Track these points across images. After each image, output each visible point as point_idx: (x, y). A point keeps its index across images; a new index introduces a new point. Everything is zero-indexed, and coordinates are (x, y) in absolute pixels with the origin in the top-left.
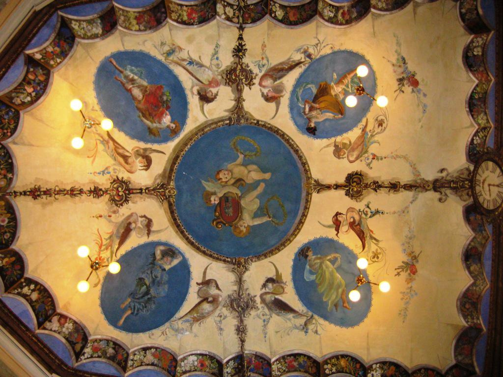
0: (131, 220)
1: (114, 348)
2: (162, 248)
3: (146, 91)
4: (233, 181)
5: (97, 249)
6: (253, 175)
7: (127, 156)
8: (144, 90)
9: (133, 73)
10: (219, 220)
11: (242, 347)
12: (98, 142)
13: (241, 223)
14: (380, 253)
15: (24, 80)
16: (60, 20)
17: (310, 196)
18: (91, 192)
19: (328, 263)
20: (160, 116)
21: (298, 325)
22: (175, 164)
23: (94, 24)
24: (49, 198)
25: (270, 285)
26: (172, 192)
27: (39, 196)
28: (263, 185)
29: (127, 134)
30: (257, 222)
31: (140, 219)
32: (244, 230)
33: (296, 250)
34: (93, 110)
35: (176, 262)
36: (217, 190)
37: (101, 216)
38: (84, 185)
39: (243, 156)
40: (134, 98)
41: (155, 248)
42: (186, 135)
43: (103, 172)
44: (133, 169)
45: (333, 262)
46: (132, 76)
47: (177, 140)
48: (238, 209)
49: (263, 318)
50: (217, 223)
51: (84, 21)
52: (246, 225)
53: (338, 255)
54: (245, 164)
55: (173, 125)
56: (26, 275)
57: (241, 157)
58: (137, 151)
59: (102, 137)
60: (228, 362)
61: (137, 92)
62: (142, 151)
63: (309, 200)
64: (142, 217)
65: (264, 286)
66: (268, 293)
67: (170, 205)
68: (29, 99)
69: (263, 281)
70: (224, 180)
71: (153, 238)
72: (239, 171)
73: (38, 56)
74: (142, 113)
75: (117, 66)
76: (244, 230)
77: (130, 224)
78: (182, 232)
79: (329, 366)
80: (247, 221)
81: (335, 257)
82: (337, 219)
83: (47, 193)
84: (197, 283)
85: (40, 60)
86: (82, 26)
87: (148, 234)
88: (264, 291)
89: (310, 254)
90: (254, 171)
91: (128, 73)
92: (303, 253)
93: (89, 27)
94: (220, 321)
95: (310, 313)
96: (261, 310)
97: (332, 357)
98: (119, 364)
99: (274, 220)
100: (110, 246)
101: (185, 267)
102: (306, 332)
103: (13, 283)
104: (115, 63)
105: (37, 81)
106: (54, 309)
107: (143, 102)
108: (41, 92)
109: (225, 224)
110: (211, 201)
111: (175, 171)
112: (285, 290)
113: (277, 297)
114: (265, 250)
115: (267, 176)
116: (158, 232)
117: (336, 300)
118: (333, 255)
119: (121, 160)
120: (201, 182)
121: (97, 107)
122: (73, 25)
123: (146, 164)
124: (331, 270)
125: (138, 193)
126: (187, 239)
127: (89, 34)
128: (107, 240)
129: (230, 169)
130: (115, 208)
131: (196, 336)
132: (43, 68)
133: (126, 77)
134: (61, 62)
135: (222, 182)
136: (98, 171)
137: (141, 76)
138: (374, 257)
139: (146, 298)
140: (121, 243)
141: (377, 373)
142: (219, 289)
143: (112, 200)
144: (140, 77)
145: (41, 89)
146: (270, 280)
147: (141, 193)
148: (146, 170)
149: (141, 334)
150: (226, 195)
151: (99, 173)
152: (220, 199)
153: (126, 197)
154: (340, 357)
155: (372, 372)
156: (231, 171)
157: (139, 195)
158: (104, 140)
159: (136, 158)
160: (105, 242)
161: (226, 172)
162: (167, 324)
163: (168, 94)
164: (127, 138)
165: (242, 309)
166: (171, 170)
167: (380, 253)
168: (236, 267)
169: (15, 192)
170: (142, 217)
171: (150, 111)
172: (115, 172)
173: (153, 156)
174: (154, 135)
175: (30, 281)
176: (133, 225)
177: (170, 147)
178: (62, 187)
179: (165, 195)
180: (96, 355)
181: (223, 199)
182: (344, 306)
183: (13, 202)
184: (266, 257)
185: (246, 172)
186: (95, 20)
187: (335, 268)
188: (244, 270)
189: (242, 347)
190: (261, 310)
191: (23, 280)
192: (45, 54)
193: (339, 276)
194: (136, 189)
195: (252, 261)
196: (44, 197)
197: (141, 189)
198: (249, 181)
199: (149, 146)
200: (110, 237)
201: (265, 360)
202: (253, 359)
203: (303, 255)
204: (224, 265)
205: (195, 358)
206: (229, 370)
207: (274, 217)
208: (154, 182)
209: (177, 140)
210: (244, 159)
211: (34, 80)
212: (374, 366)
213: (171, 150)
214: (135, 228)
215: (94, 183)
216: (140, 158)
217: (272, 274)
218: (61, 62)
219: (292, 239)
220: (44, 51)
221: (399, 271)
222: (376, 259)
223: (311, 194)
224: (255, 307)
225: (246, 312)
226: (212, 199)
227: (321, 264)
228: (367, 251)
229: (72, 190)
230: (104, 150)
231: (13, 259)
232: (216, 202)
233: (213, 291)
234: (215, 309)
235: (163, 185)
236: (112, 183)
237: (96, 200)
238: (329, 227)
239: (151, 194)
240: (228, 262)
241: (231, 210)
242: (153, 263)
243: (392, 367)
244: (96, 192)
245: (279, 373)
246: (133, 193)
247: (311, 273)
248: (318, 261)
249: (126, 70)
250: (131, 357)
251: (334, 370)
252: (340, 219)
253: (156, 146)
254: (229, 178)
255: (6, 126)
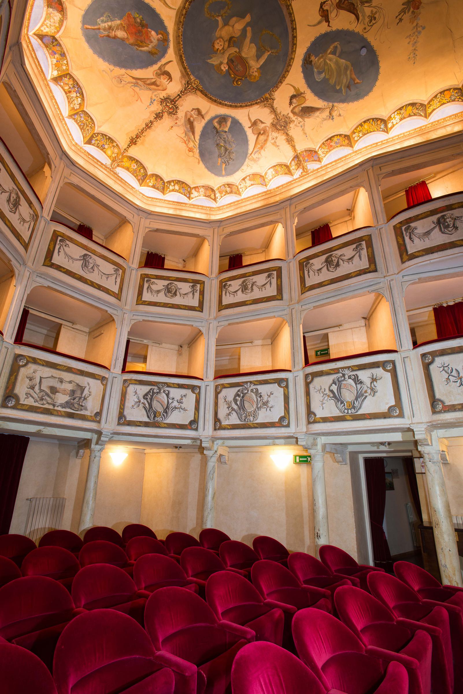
0: (188, 117)
1: (229, 187)
2: (216, 120)
3: (124, 27)
4: (227, 44)
5: (184, 145)
6: (238, 26)
7: (154, 82)
8: (120, 27)
9: (105, 22)
10: (237, 79)
11: (295, 150)
12: (133, 87)
13: (251, 70)
14: (376, 13)
15: (66, 93)
16: (36, 37)
17: (290, 7)
18: (156, 118)
19: (330, 56)
20: (148, 37)
21: (325, 117)
22: (183, 62)
23: (51, 15)
24: (141, 139)
25: (294, 101)
26: (196, 83)
27: (136, 141)
28: (249, 29)
29: (141, 68)
30: (262, 61)
31: (192, 113)
32: (256, 74)
33: (301, 63)
34: (111, 71)
35: (229, 124)
36: (221, 60)
37: (172, 127)
38: (149, 118)
39: (220, 17)
40: (123, 40)
41: (212, 123)
42: (173, 36)
43: (151, 102)
44: (164, 86)
45: (334, 53)
46: (106, 25)
47: (171, 45)
48: (243, 62)
49: (300, 125)
50: (237, 82)
51: (45, 21)
52: (256, 70)
53: (336, 43)
54: (226, 23)
55: (160, 36)
56: (166, 181)
57: (219, 19)
58: (156, 73)
59: (132, 83)
60: (291, 163)
61: (121, 34)
62: (159, 71)
63: (291, 12)
64: (192, 111)
65: (291, 103)
66: (296, 107)
67: (201, 91)
68: (79, 99)
69: (288, 101)
70: (220, 48)
71: (207, 118)
72: (225, 32)
73: (55, 73)
74: (137, 45)
75: (93, 27)
76: (256, 74)
77: (189, 119)
78: (220, 103)
79: (357, 134)
80: (255, 65)
81: (334, 47)
82: (324, 10)
83: (138, 137)
84: (249, 127)
85: (58, 74)
86: (48, 25)
87: (203, 118)
88: (292, 107)
89: (313, 58)
90: (236, 23)
91: (103, 25)
92: (307, 63)
93: (52, 20)
94: (275, 142)
95: (331, 104)
96: (296, 121)
97: (358, 127)
98: (235, 193)
99: (272, 51)
100: (189, 139)
101: (236, 123)
102: (333, 119)
103: (163, 189)
104: (90, 27)
105: (71, 87)
106: (190, 187)
107: (129, 37)
108: (79, 90)
109: (241, 79)
110: (222, 70)
111: (187, 67)
112: (306, 98)
113: (302, 106)
114: (279, 77)
115: (248, 18)
116: (207, 113)
117: (348, 83)
118: (332, 47)
119: (153, 87)
120: (208, 63)
121: (112, 67)
122: (45, 31)
123: (168, 77)
124: (335, 60)
125: (178, 99)
126: (226, 105)
127: (57, 25)
128: (185, 137)
129: (219, 36)
130: (175, 116)
131: (266, 157)
132: (65, 76)
133: (105, 29)
134: (67, 62)
135: (220, 51)
136: (149, 104)
137: (111, 19)
138: (371, 21)
139: (227, 153)
140: (193, 133)
141: (396, 119)
142: (264, 123)
143: (170, 113)
144: (112, 21)
145: (78, 88)
146: (293, 97)
147: (180, 97)
148: (171, 81)
149: (237, 173)
150: (230, 58)
151: (150, 105)
152: (227, 63)
153: (175, 106)
154: (363, 124)
155: (391, 121)
156: (221, 37)
157: (180, 99)
158: (134, 84)
159: (160, 78)
160: (185, 139)
161: (218, 41)
162: (247, 160)
163: (138, 16)
164: (144, 70)
165: (285, 127)
166: (185, 68)
167: (376, 13)
168: (266, 102)
169: (125, 149)
170: (192, 111)
171: (140, 39)
172: (157, 97)
173: (167, 68)
174: (156, 54)
175: (169, 182)
176: (192, 119)
177: (171, 54)
178: (141, 128)
179: (194, 88)
180: (223, 195)
181: (229, 62)
182: (355, 84)
183: (129, 155)
184: (282, 83)
185: (231, 28)
186: (48, 12)
187: (338, 57)
188: (272, 101)
189: (295, 150)
190: (296, 121)
191: (166, 184)
192: (57, 66)
193: (344, 61)
194: (176, 97)
195: (273, 92)
196: (138, 140)
197: (179, 95)
198: (237, 34)
199: (159, 64)
200: (186, 134)
201: (312, 151)
202: (305, 154)
203: (307, 63)
204: (258, 106)
205: (272, 170)
206: (293, 167)
207: (271, 48)
208: (182, 85)
209: (171, 45)
210: (223, 19)
211: (70, 88)
212: (392, 116)
213: (174, 56)
214: (194, 120)
215: (153, 112)
216: (162, 77)
217: (292, 92)
218: (67, 62)
219: (293, 57)
220: (54, 66)
221: (400, 17)
222: (373, 22)
223: (291, 5)
224: (291, 121)
225: (287, 127)
226: (223, 68)
227: (325, 60)
228: (362, 20)
229: (147, 125)
230: (140, 90)
231: (154, 178)
232: (227, 68)
233: (261, 126)
234: (268, 136)
235: (188, 82)
236: (161, 105)
237: (162, 120)
238: (319, 23)
239: (186, 93)
240: (259, 102)
241: (239, 66)
242: (217, 132)
243: (410, 108)
244: (159, 116)
245: (324, 155)
246: (176, 101)
247: (320, 73)
248: (322, 60)
249: (99, 24)
250: (239, 187)
251: (361, 135)
252: (325, 8)
253: (163, 61)
254: (222, 44)
255: (88, 123)
